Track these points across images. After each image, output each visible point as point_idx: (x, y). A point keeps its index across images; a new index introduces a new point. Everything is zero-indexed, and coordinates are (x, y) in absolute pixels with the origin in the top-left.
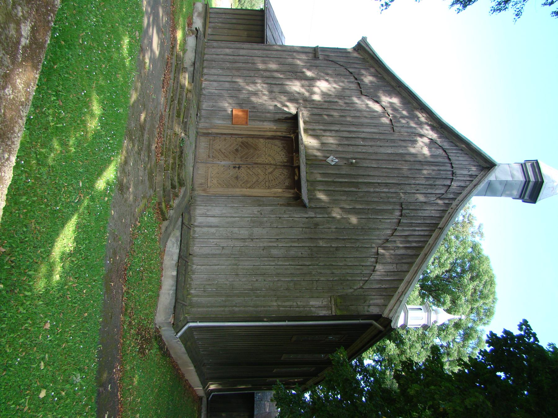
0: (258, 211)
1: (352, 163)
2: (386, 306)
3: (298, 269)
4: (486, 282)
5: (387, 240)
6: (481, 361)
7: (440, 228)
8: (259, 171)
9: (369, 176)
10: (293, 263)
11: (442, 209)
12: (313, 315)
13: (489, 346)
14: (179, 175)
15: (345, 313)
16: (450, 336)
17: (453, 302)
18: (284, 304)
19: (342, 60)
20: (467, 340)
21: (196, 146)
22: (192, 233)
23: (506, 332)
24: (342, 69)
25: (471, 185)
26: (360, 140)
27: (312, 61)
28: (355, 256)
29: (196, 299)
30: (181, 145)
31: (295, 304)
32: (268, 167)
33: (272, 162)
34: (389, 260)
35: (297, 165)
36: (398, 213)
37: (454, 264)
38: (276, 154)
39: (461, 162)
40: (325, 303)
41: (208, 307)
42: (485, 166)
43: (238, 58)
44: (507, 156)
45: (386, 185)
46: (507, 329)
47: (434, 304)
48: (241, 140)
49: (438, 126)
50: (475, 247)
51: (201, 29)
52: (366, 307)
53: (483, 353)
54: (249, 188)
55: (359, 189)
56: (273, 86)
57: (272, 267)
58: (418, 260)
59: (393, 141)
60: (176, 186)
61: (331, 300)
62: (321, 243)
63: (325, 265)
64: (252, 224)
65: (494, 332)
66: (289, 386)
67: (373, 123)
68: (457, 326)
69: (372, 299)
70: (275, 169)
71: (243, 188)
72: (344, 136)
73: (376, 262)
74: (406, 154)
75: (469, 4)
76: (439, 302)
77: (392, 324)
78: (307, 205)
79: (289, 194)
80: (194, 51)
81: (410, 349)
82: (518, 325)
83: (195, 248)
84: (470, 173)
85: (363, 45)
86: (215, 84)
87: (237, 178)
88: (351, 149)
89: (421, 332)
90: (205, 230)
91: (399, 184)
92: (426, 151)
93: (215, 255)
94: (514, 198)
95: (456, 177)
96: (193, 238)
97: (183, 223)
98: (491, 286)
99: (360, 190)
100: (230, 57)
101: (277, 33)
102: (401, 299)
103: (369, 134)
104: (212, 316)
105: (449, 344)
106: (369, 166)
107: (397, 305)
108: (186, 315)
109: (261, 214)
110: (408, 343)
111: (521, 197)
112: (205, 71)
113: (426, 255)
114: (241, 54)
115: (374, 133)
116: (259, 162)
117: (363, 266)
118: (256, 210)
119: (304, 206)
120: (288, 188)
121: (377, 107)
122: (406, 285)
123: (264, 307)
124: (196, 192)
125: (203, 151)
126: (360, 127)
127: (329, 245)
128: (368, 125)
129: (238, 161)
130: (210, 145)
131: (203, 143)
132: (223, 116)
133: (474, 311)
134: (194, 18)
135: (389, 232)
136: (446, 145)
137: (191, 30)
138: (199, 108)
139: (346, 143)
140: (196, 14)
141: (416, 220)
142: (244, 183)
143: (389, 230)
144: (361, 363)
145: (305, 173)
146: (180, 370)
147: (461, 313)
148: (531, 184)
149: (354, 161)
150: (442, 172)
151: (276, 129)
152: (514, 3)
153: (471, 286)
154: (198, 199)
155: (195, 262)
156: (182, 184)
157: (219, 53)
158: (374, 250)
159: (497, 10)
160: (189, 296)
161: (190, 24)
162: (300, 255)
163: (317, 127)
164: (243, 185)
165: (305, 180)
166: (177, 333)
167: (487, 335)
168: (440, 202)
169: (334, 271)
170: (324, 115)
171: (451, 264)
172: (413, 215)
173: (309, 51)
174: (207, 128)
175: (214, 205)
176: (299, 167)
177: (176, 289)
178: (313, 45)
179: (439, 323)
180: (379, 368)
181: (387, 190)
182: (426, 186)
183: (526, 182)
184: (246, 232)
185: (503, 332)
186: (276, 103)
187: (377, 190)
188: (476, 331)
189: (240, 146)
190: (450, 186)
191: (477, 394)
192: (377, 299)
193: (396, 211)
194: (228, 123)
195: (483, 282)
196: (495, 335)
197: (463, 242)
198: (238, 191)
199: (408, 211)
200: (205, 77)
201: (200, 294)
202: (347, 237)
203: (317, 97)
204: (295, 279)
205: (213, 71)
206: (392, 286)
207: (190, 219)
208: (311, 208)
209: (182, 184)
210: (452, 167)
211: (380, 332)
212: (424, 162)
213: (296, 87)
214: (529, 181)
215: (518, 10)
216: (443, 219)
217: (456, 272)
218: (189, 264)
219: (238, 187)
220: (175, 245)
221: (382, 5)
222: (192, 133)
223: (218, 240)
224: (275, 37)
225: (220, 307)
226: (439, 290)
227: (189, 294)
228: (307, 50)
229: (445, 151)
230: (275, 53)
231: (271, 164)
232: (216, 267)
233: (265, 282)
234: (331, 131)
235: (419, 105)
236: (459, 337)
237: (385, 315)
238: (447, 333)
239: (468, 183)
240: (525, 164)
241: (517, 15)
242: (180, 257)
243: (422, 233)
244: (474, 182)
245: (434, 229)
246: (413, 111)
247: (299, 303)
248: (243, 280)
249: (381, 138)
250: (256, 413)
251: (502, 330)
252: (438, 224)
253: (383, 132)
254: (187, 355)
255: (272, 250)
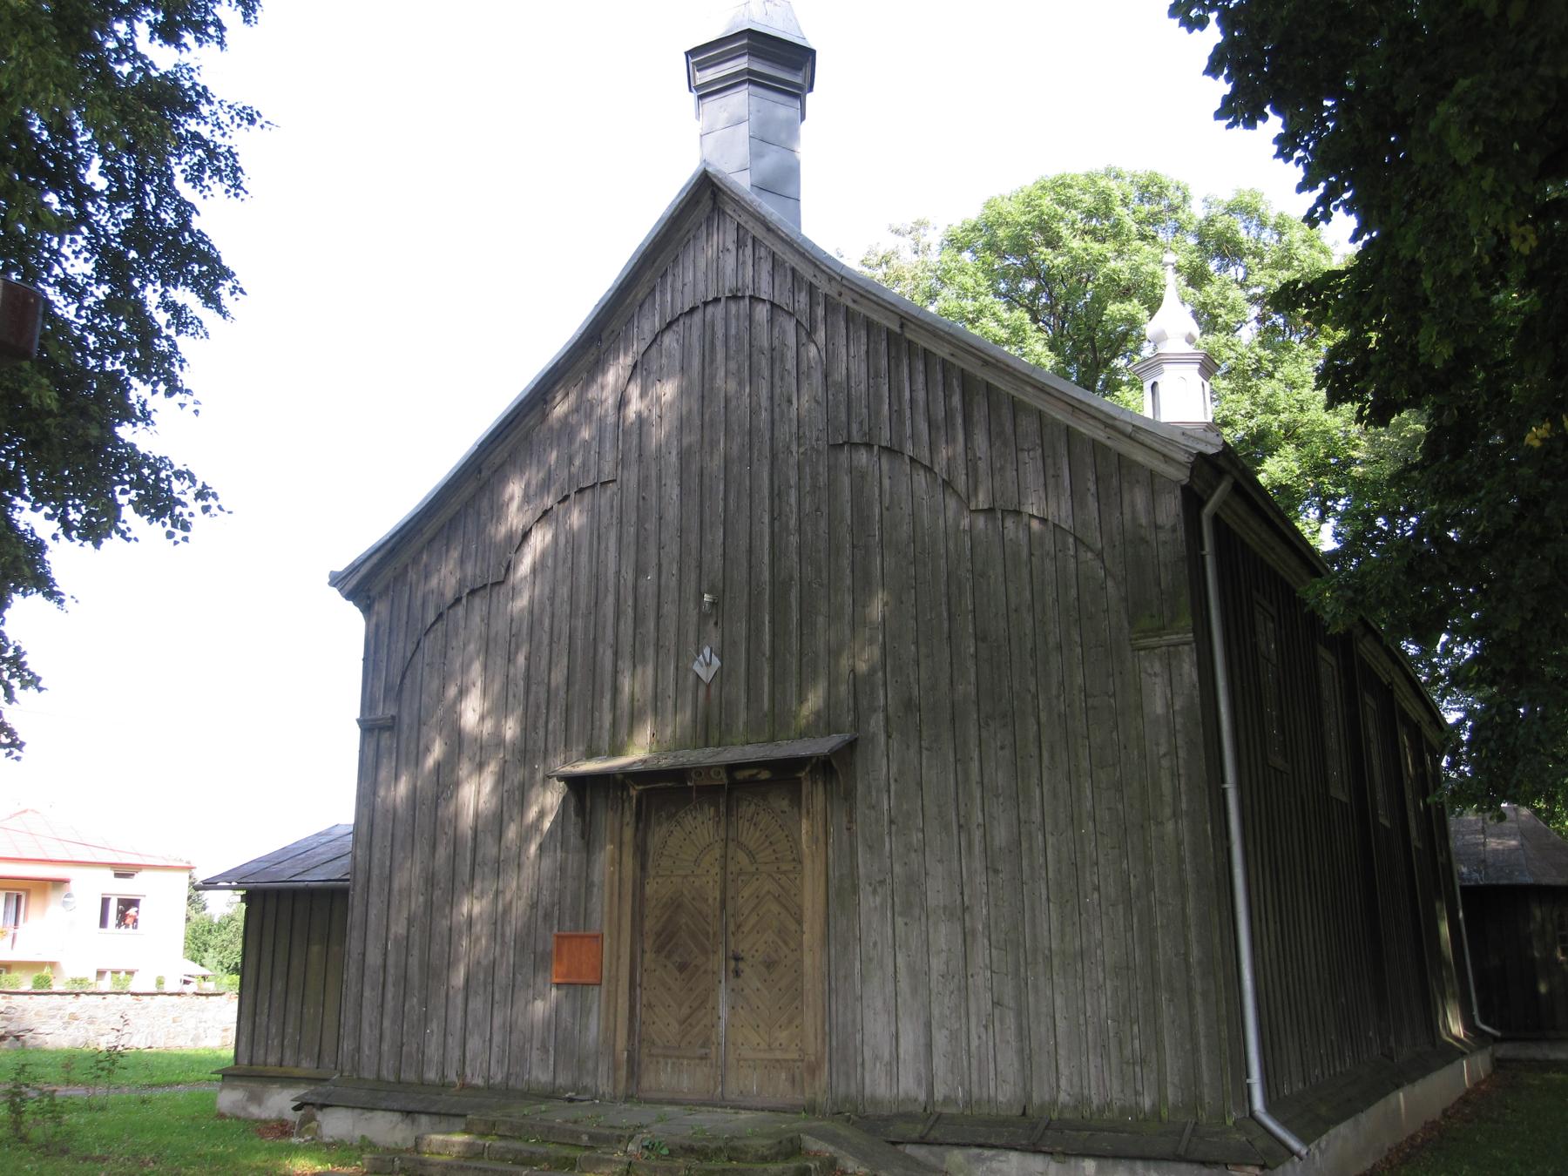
0: (875, 892)
1: (713, 604)
2: (1152, 474)
3: (1052, 757)
4: (1061, 203)
5: (948, 484)
6: (1312, 153)
7: (902, 326)
8: (746, 893)
9: (750, 551)
10: (1036, 774)
11: (843, 324)
12: (1197, 700)
13: (1265, 118)
14: (764, 1159)
15: (1185, 600)
16: (1230, 294)
17: (1126, 294)
18: (1168, 798)
19: (401, 644)
20: (1238, 244)
21: (672, 1102)
22: (952, 1110)
23: (1213, 69)
24: (427, 644)
25: (769, 241)
26: (642, 582)
27: (404, 737)
28: (1001, 579)
29: (1170, 1091)
30: (665, 1151)
31: (1165, 763)
32: (732, 867)
33: (717, 852)
34: (1010, 474)
35: (723, 775)
36: (862, 457)
37: (1012, 300)
38: (691, 844)
39: (700, 275)
40: (1157, 667)
41: (1195, 1049)
42: (710, 203)
43: (391, 970)
44: (674, 142)
45: (777, 495)
46: (1205, 63)
47: (1137, 351)
48: (649, 956)
49: (593, 350)
50: (957, 244)
51: (300, 1091)
52: (1162, 536)
53: (1285, 146)
54: (800, 922)
55: (791, 578)
56: (479, 859)
57: (1050, 840)
58: (1003, 385)
59: (643, 484)
60: (798, 1169)
61: (1144, 649)
62: (966, 688)
63: (1034, 672)
64: (916, 911)
65: (1218, 106)
66: (1429, 780)
67: (591, 544)
68: (1197, 278)
69: (1134, 519)
70: (740, 845)
71: (801, 944)
72: (630, 632)
73: (1018, 513)
74: (680, 441)
75: (218, 260)
76: (1125, 338)
77: (1211, 451)
78: (847, 736)
79: (816, 795)
80: (368, 1115)
81: (1278, 413)
82: (1190, 31)
83: (1000, 1098)
84: (732, 247)
85: (354, 582)
86: (474, 1043)
87: (770, 965)
88: (669, 609)
89: (1224, 384)
90: (939, 1063)
91: (774, 457)
92: (668, 390)
93: (1020, 1027)
94: (803, 118)
95: (745, 287)
96: (968, 1103)
97: (922, 1141)
98: (1070, 187)
99: (796, 575)
100: (389, 996)
101: (320, 850)
102: (1129, 429)
103: (624, 562)
104: (1224, 1034)
105: (1253, 300)
106: (720, 551)
107: (1148, 441)
108: (1230, 1122)
109: (882, 882)
110: (1260, 419)
111: (797, 93)
112: (431, 1075)
113: (986, 363)
114: (379, 961)
115: (620, 539)
116: (718, 894)
117: (1031, 554)
118: (869, 901)
119: (852, 745)
120: (796, 801)
121: (540, 539)
122: (1083, 416)
123: (1181, 860)
124: (819, 1099)
125: (687, 1079)
126: (602, 584)
127: (970, 664)
128: (597, 558)
129: (718, 961)
130: (666, 1057)
131: (661, 1078)
132: (574, 1016)
133: (1149, 230)
134: (264, 1115)
135: (921, 478)
136: (649, 324)
137: (302, 1124)
138: (550, 1095)
139: (652, 625)
140: (255, 1111)
141: (879, 397)
142: (786, 943)
143: (915, 477)
144: (1333, 556)
145: (747, 748)
146: (1413, 1138)
147: (1158, 269)
148: (758, 67)
149: (707, 598)
150: (733, 331)
151: (612, 842)
152: (218, 132)
153: (1076, 244)
154: (842, 1090)
155: (1047, 1098)
156: (791, 1149)
157: (377, 1032)
158: (981, 522)
159: (236, 178)
160: (1165, 1113)
161: (282, 1129)
162: (1007, 753)
163: (607, 719)
164: (792, 945)
165: (770, 746)
166: (1292, 1153)
167: (1230, 126)
168: (821, 336)
169: (1052, 641)
170: (565, 697)
171: (1011, 309)
172: (865, 411)
173: (373, 745)
174: (615, 1067)
175: (859, 1036)
176: (732, 768)
177: (1144, 1158)
178: (352, 736)
179: (1196, 330)
180: (1342, 501)
181: (793, 494)
182: (777, 377)
183: (751, 82)
184: (943, 929)
185: (1216, 77)
186: (533, 849)
187: (793, 522)
188: (1211, 221)
189: (668, 957)
190: (772, 304)
191: (1433, 125)
192: (1133, 505)
193: (855, 463)
194: (596, 998)
195: (1061, 210)
196: (1227, 100)
197: (944, 277)
198: (811, 961)
199: (855, 427)
200: (452, 1076)
201: (1153, 1076)
202: (944, 607)
203: (511, 729)
204: (1085, 764)
205: (433, 1051)
206: (1089, 460)
207: (908, 1117)
208: (856, 724)
209: (791, 1149)
210: (717, 300)
211: (1237, 489)
212: (701, 393)
213: (475, 794)
214: (749, 72)
215: (237, 119)
216: (875, 317)
217: (1034, 294)
218: (1055, 1116)
219: (801, 960)
220: (995, 1165)
221: (206, 509)
222: (627, 1116)
223: (973, 1020)
224: (331, 856)
225: (1191, 1007)
226: (1092, 340)
227: (1156, 1112)
228: (371, 753)
229: (669, 325)
230: (377, 855)
231: (724, 856)
232: (1061, 1025)
233: (1102, 860)
234: (616, 672)
235: (532, 409)
236: (1232, 270)
237: (1183, 476)
238: (1221, 305)
239: (763, 253)
240: (698, 88)
241: (252, 121)
242: (1035, 1150)
243: (920, 379)
244: (759, 232)
245: (905, 345)
246: (551, 429)
247: (1162, 750)
248: (1098, 935)
249: (634, 519)
250: (1529, 880)
251: (1209, 79)
252: (889, 332)
253: (615, 513)
254: (1363, 1117)
255: (997, 843)
